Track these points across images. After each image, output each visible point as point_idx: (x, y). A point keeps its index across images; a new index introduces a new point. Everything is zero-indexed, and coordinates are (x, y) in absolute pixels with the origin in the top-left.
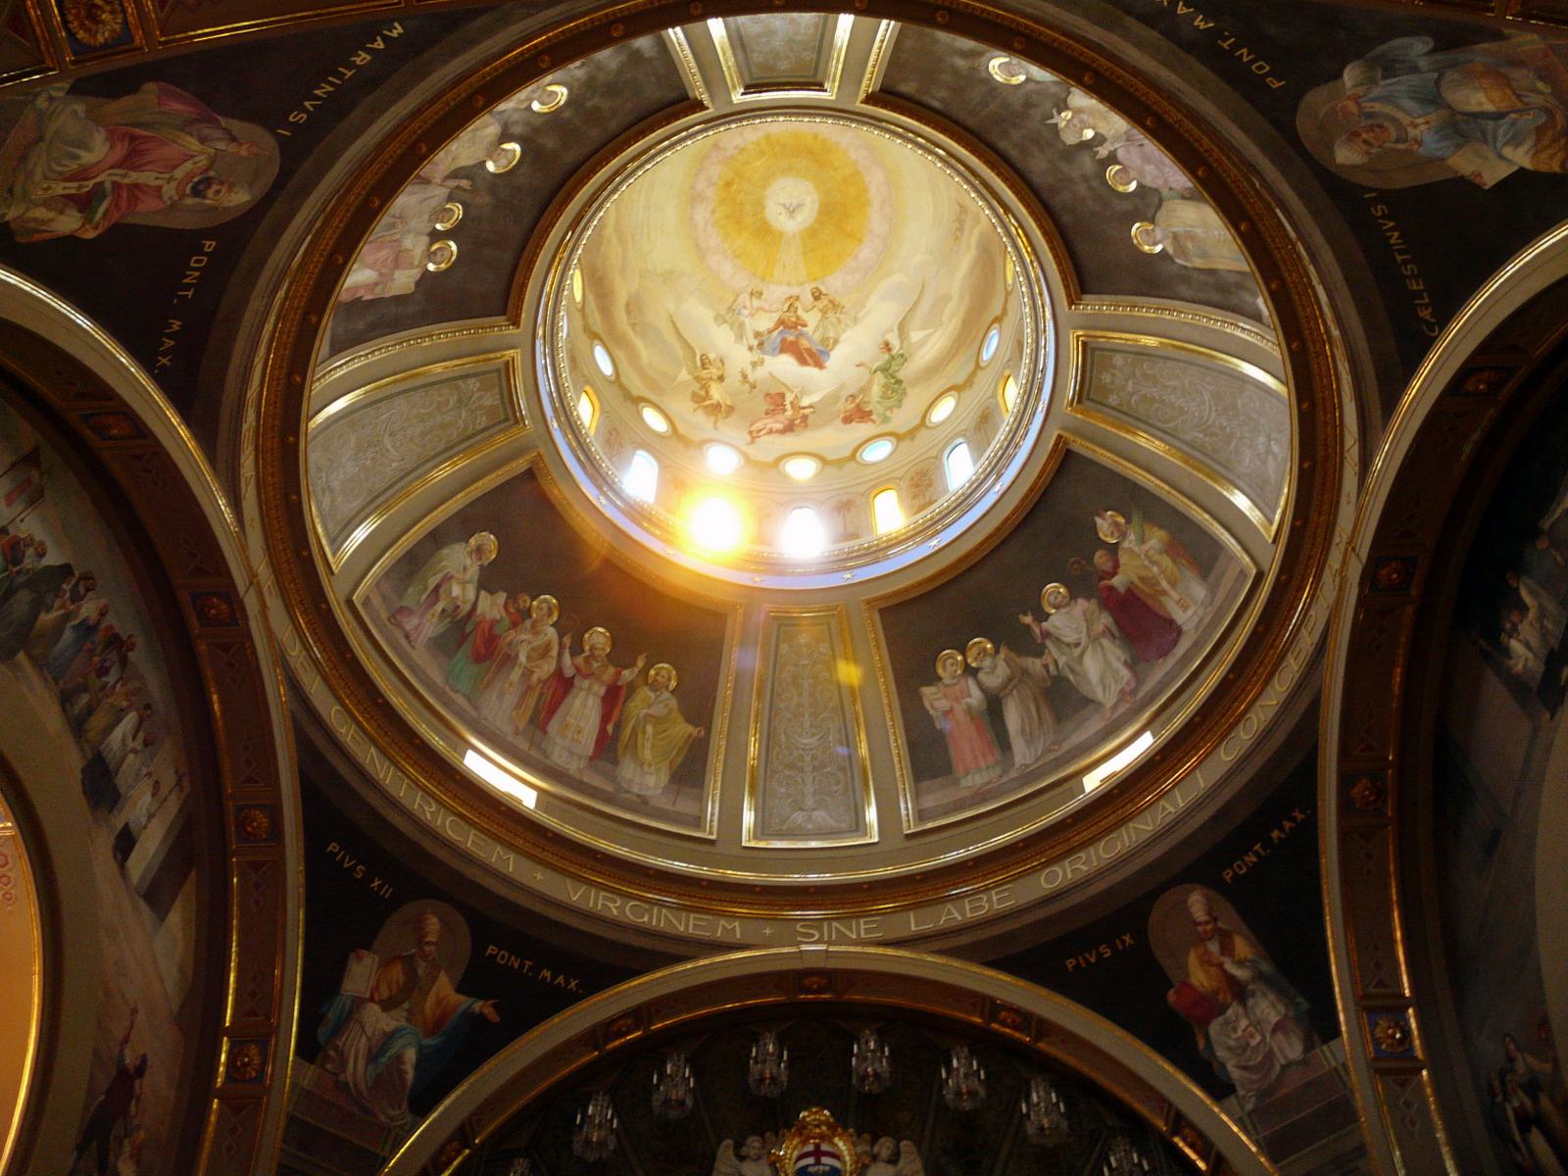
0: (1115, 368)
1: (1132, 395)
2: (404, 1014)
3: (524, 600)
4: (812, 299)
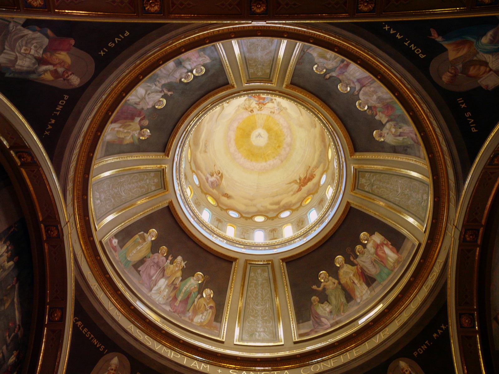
0: (154, 185)
1: (147, 179)
2: (477, 55)
3: (369, 113)
4: (254, 110)
